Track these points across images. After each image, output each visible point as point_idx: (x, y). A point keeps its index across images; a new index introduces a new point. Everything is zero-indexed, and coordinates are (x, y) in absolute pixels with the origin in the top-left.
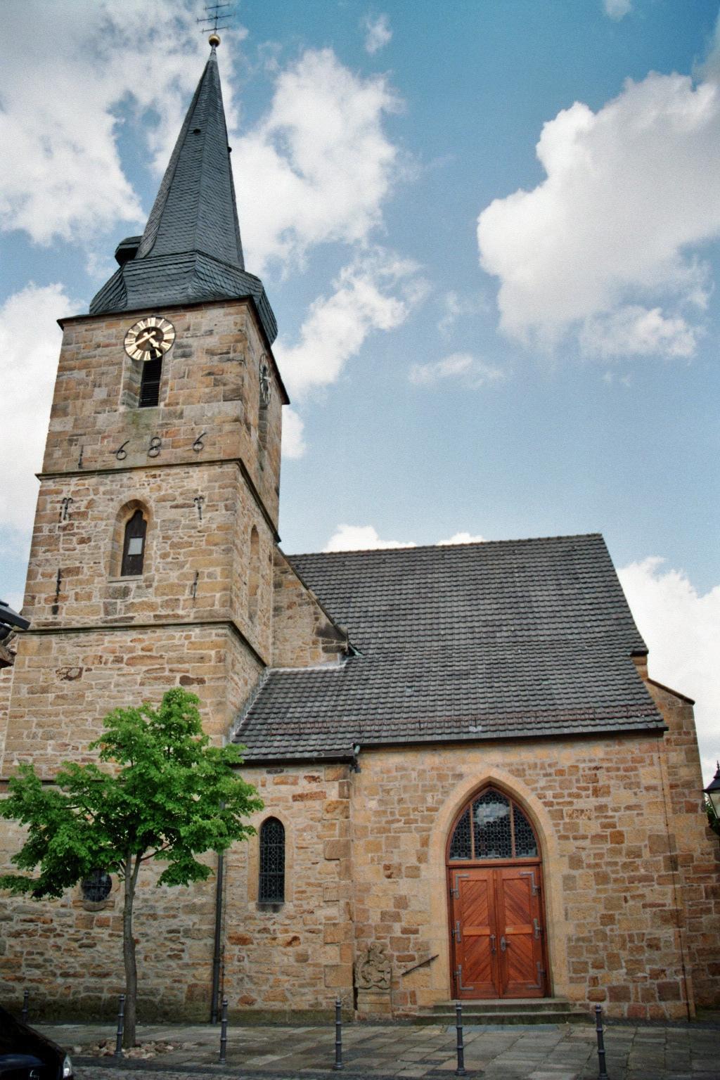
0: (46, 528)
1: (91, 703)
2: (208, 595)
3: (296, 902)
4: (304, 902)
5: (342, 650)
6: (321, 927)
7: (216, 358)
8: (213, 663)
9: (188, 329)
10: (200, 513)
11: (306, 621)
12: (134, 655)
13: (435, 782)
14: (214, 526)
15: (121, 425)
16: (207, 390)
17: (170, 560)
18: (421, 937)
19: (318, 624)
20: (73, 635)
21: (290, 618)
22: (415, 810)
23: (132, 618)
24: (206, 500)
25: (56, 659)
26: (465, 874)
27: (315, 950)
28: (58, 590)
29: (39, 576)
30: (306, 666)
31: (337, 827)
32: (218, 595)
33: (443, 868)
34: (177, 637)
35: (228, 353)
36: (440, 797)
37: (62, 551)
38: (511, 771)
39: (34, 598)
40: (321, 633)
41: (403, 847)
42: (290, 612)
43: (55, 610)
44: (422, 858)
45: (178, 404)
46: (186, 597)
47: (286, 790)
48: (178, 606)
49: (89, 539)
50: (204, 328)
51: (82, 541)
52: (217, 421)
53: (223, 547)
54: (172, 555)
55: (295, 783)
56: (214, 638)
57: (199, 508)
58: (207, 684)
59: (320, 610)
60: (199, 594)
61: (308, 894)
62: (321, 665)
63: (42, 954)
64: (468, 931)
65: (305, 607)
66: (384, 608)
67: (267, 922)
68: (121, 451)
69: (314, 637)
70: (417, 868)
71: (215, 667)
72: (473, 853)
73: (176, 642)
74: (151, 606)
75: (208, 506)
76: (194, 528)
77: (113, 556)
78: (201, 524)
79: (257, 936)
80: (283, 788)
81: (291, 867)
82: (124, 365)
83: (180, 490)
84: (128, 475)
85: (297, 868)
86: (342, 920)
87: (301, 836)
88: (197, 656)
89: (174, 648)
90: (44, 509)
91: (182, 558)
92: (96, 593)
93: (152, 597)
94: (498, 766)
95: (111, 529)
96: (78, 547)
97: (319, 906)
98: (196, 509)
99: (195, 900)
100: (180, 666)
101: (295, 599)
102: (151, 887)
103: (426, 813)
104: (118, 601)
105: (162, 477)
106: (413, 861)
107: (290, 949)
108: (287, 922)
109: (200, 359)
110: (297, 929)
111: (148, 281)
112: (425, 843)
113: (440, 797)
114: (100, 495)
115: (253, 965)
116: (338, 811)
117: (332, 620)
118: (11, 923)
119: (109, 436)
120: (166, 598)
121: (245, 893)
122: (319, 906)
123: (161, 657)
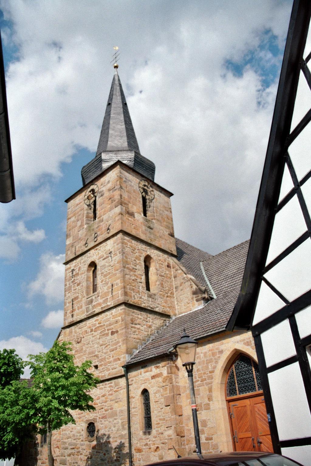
0: (68, 283)
1: (85, 351)
2: (117, 293)
3: (157, 429)
4: (159, 429)
5: (204, 299)
6: (166, 441)
7: (111, 191)
8: (120, 323)
9: (102, 184)
10: (111, 258)
11: (188, 289)
12: (96, 327)
13: (212, 357)
14: (116, 262)
15: (85, 233)
16: (110, 206)
17: (104, 282)
18: (214, 442)
19: (192, 290)
20: (78, 325)
21: (182, 290)
22: (204, 373)
23: (94, 311)
24: (113, 252)
25: (74, 336)
26: (237, 403)
27: (165, 453)
28: (73, 307)
29: (67, 304)
30: (191, 310)
31: (168, 389)
32: (120, 292)
33: (225, 402)
34: (108, 315)
35: (115, 187)
36: (214, 364)
37: (73, 291)
38: (245, 344)
39: (66, 313)
40: (194, 293)
41: (201, 394)
42: (181, 288)
43: (72, 316)
44: (210, 399)
45: (101, 216)
46: (110, 296)
47: (149, 375)
48: (107, 301)
49: (80, 283)
50: (107, 181)
51: (78, 285)
52: (114, 217)
53: (120, 270)
54: (104, 280)
55: (151, 371)
56: (120, 311)
57: (111, 257)
58: (119, 333)
59: (192, 283)
60: (114, 294)
61: (161, 424)
62: (196, 308)
63: (77, 463)
64: (241, 435)
65: (186, 283)
66: (234, 271)
67: (147, 440)
68: (86, 243)
69: (192, 296)
70: (208, 404)
71: (121, 324)
72: (238, 392)
73: (108, 317)
74: (99, 304)
75: (114, 254)
76: (110, 266)
77: (88, 287)
78: (112, 264)
79: (144, 447)
80: (147, 374)
81: (153, 412)
82: (85, 209)
83: (105, 252)
84: (89, 252)
85: (155, 412)
86: (174, 436)
87: (155, 396)
88: (115, 321)
89: (108, 320)
90: (67, 277)
91: (107, 280)
92: (84, 305)
93: (100, 301)
94: (238, 342)
95: (86, 276)
96: (77, 288)
97: (165, 430)
98: (110, 258)
99: (122, 433)
100: (110, 327)
101: (182, 281)
102: (108, 429)
103: (209, 374)
104: (90, 306)
105: (99, 249)
106: (206, 401)
107: (156, 453)
108: (154, 439)
109: (107, 194)
110: (158, 443)
111: (90, 172)
112: (210, 390)
113: (214, 364)
114: (82, 264)
115: (144, 462)
116: (167, 381)
117: (197, 286)
118: (67, 450)
119: (83, 239)
120: (104, 299)
121: (138, 427)
122: (165, 430)
123: (104, 325)
